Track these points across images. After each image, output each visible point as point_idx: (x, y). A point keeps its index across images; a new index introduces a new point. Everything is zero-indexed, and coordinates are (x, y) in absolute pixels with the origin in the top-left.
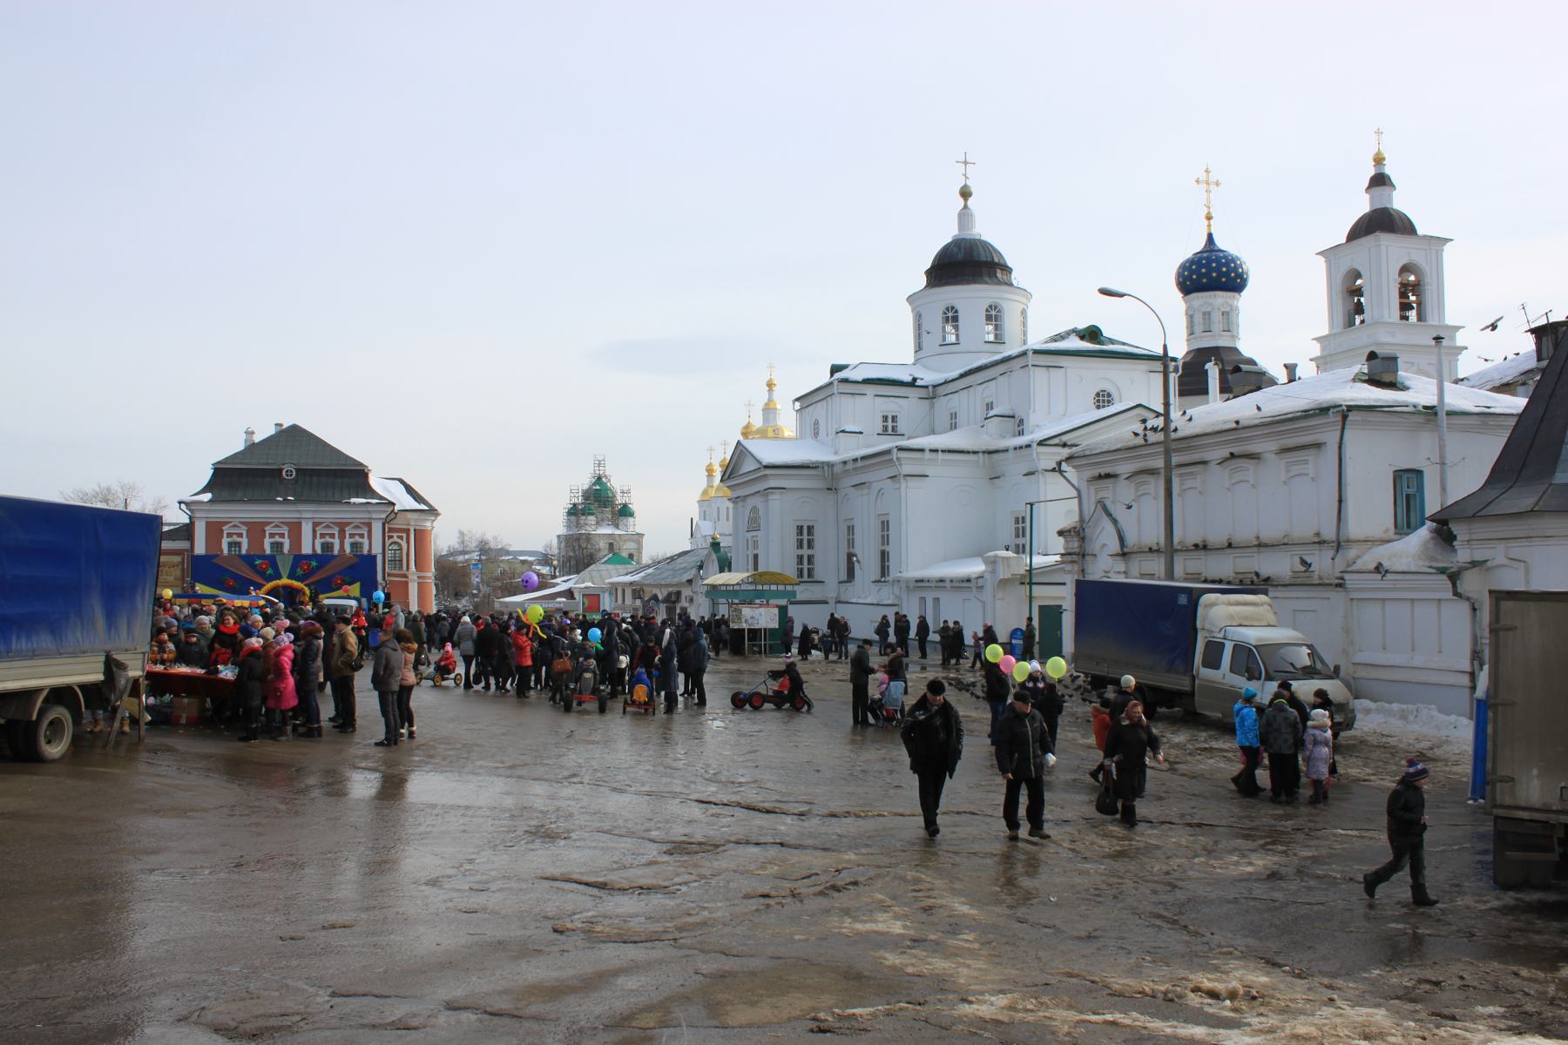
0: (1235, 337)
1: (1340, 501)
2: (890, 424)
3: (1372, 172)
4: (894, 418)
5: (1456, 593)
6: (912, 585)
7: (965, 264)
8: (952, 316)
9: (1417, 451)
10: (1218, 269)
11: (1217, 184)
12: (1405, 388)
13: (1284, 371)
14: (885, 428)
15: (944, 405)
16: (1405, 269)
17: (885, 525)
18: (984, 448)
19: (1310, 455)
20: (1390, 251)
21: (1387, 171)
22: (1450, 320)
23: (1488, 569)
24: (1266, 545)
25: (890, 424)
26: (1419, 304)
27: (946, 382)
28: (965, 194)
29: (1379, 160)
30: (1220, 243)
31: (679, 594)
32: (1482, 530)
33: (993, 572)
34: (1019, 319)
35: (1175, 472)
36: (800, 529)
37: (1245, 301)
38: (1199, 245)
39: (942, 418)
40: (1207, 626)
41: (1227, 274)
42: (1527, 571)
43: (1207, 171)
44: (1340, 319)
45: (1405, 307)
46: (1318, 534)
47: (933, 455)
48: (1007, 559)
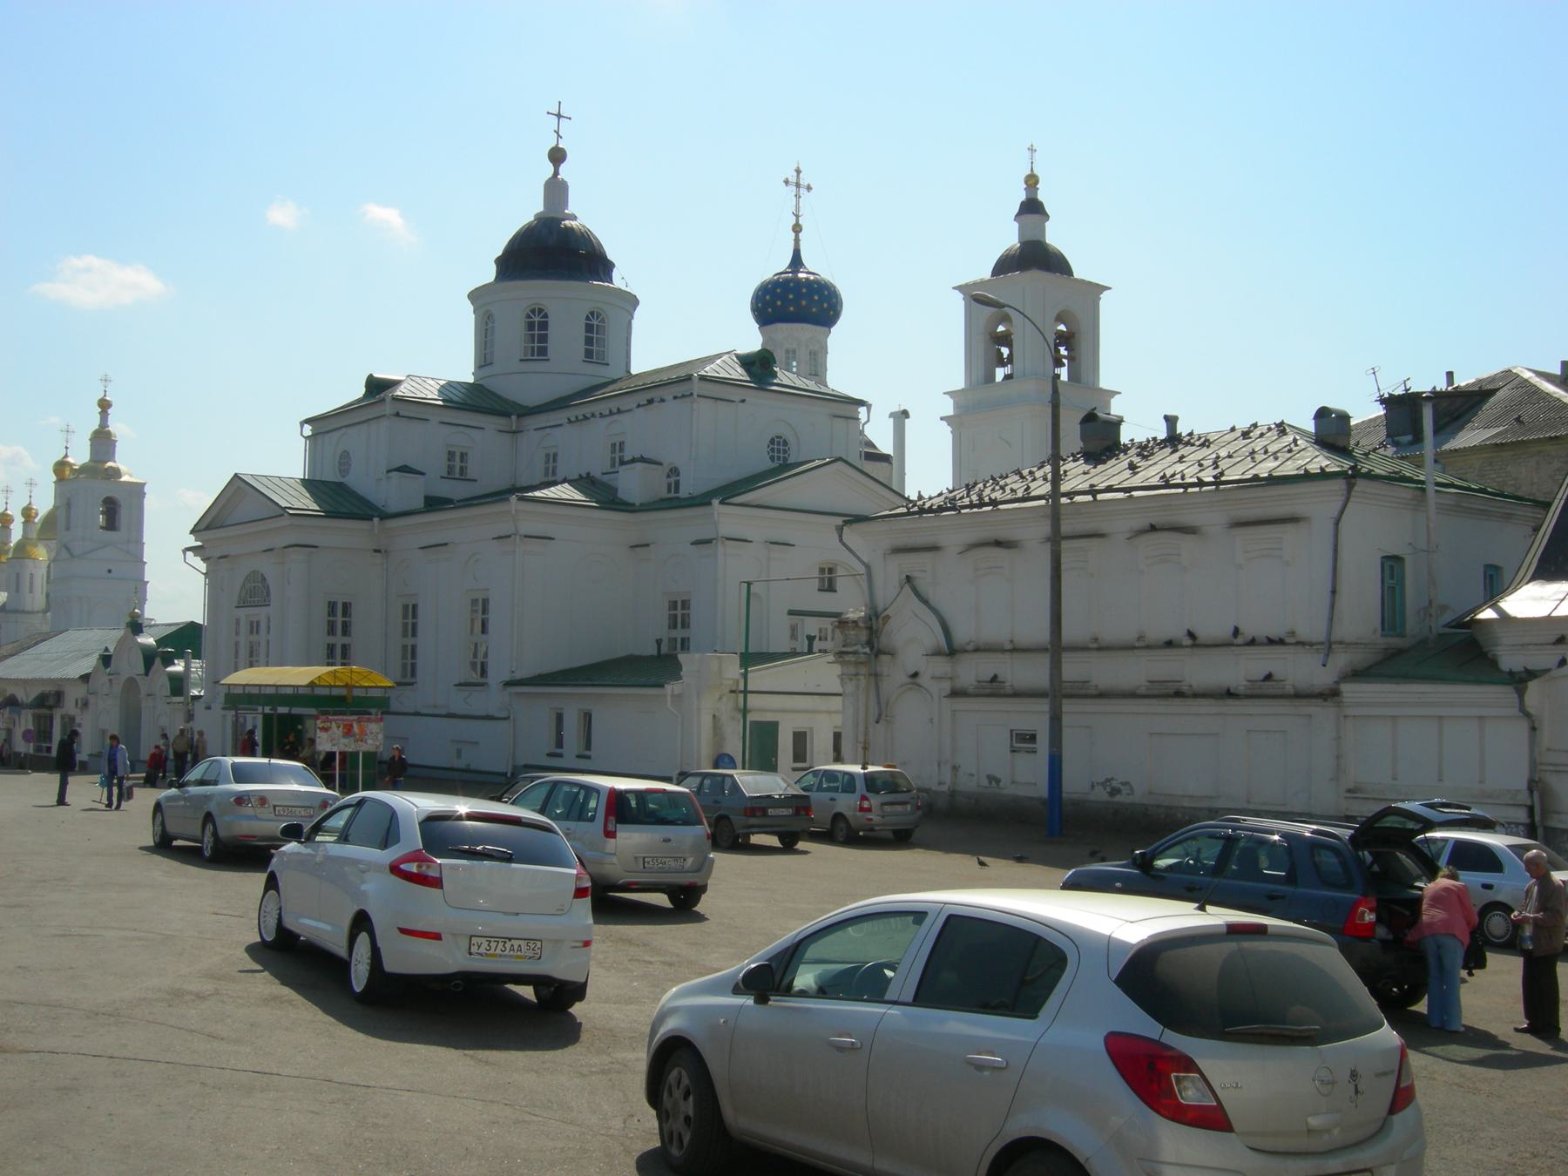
2: (457, 463)
3: (1023, 197)
4: (463, 456)
7: (553, 253)
8: (538, 326)
11: (809, 188)
13: (1163, 425)
14: (450, 469)
19: (1288, 533)
25: (457, 463)
28: (557, 156)
29: (1032, 181)
31: (59, 696)
35: (1065, 545)
36: (332, 607)
38: (782, 263)
43: (798, 171)
46: (1293, 633)
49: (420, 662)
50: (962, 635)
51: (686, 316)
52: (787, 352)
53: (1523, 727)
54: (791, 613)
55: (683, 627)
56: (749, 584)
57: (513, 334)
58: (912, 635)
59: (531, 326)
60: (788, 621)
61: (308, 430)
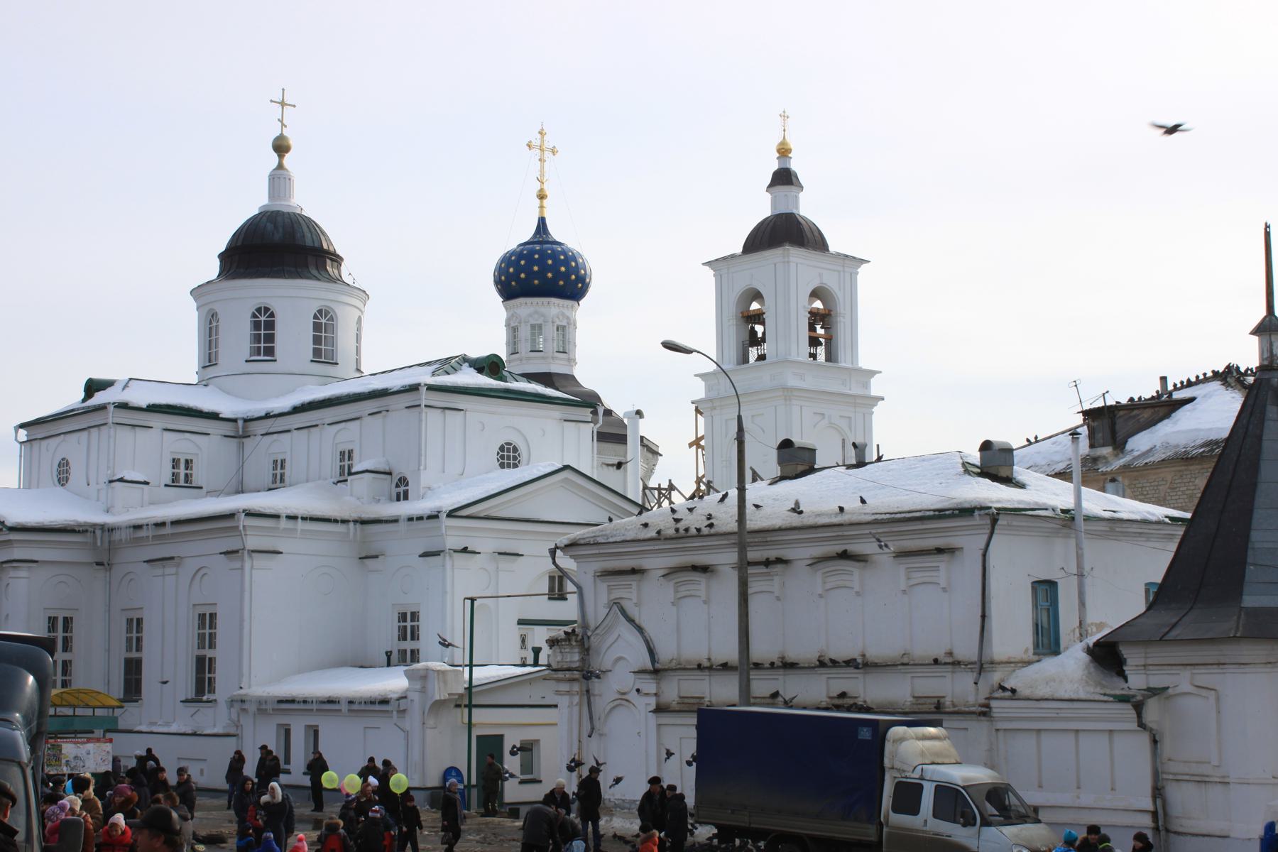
0: (571, 361)
1: (983, 616)
4: (188, 463)
5: (1142, 725)
6: (269, 707)
7: (276, 248)
8: (264, 330)
9: (1053, 559)
10: (555, 269)
11: (554, 151)
12: (1022, 486)
14: (175, 477)
15: (262, 450)
16: (815, 294)
17: (207, 620)
18: (355, 516)
19: (941, 562)
20: (794, 272)
21: (794, 166)
22: (864, 362)
23: (1171, 696)
24: (876, 665)
26: (829, 340)
27: (268, 416)
28: (281, 147)
29: (784, 152)
30: (556, 232)
32: (1159, 654)
33: (423, 691)
34: (355, 326)
37: (586, 313)
38: (526, 233)
39: (259, 468)
40: (898, 765)
41: (566, 276)
42: (1218, 699)
44: (732, 353)
45: (814, 342)
46: (950, 654)
47: (290, 524)
48: (443, 672)
49: (145, 635)
50: (666, 652)
51: (417, 303)
52: (533, 327)
53: (1145, 739)
54: (521, 622)
55: (412, 639)
56: (473, 600)
57: (237, 338)
58: (621, 653)
59: (256, 325)
60: (515, 632)
61: (23, 435)
